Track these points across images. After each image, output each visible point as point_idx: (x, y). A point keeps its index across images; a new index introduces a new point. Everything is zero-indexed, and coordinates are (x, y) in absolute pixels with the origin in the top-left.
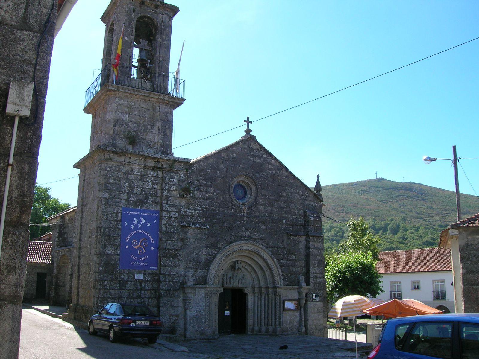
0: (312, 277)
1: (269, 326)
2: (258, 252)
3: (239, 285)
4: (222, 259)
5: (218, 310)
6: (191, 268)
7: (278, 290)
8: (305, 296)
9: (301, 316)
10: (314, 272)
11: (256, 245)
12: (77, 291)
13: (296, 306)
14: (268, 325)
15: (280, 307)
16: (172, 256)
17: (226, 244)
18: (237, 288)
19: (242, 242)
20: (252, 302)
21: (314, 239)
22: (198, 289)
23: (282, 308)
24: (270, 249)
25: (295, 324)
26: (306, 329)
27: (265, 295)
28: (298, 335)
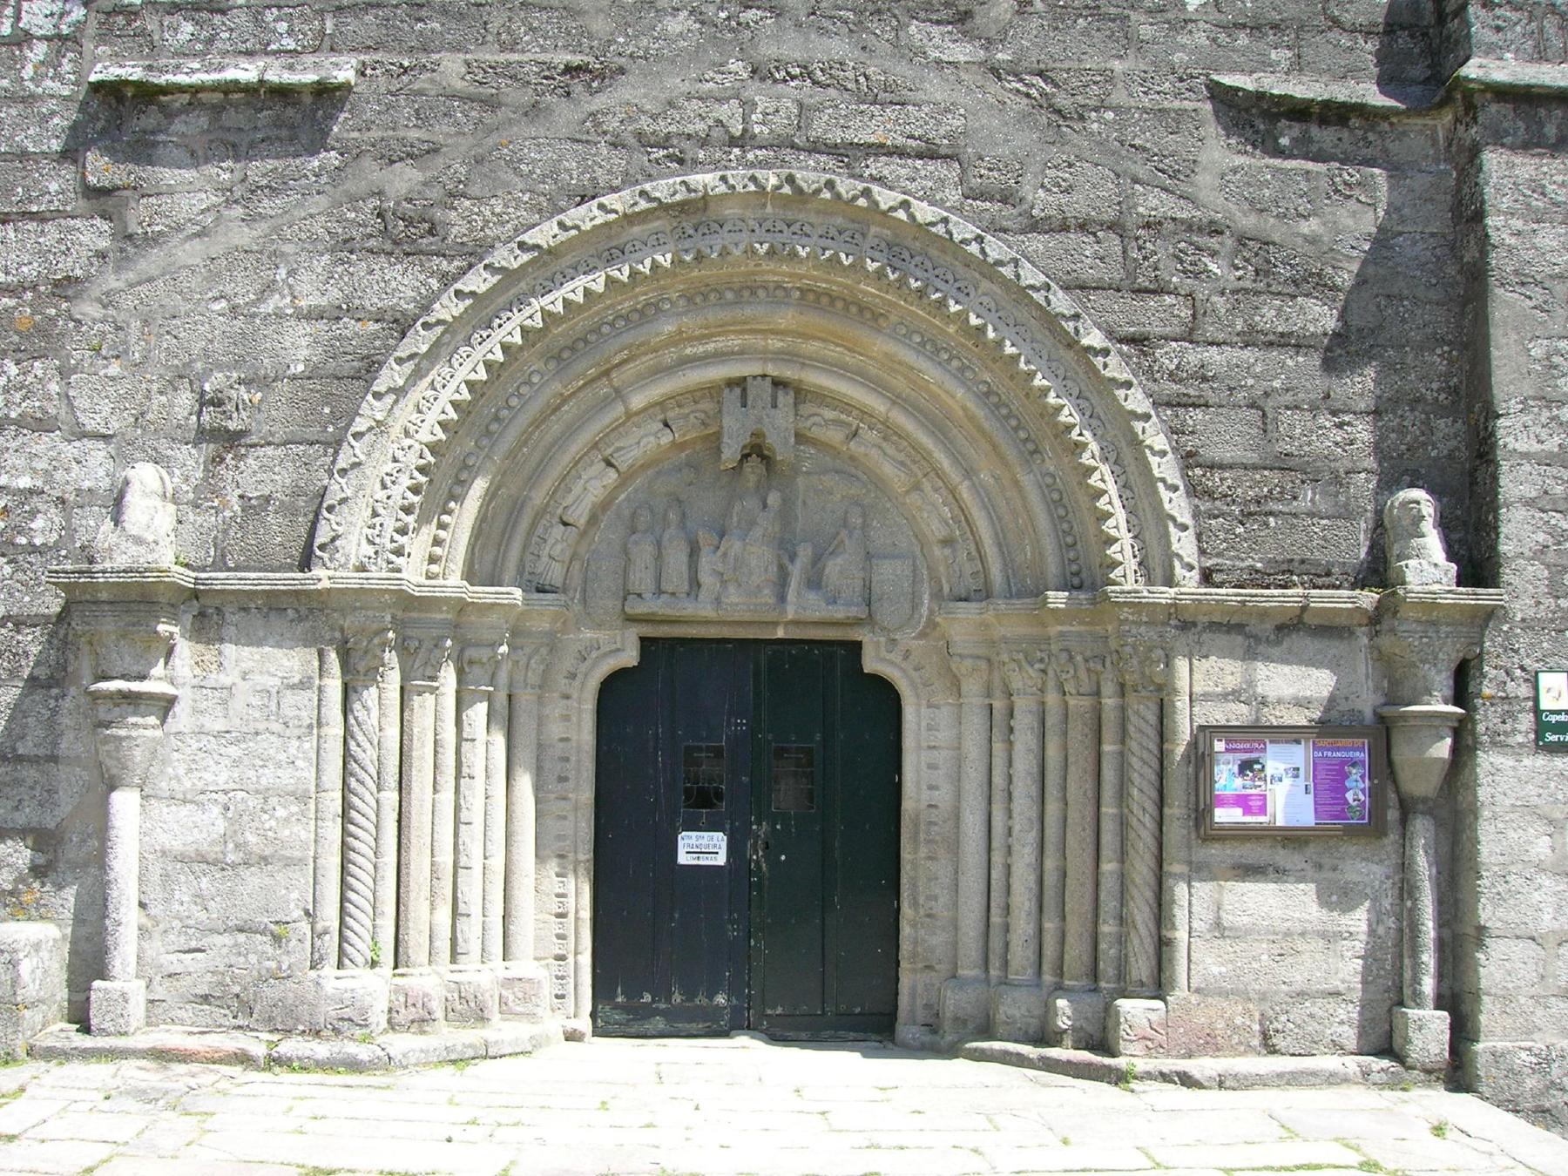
0: (1529, 503)
9: (1411, 896)
12: (991, 944)
16: (16, 338)
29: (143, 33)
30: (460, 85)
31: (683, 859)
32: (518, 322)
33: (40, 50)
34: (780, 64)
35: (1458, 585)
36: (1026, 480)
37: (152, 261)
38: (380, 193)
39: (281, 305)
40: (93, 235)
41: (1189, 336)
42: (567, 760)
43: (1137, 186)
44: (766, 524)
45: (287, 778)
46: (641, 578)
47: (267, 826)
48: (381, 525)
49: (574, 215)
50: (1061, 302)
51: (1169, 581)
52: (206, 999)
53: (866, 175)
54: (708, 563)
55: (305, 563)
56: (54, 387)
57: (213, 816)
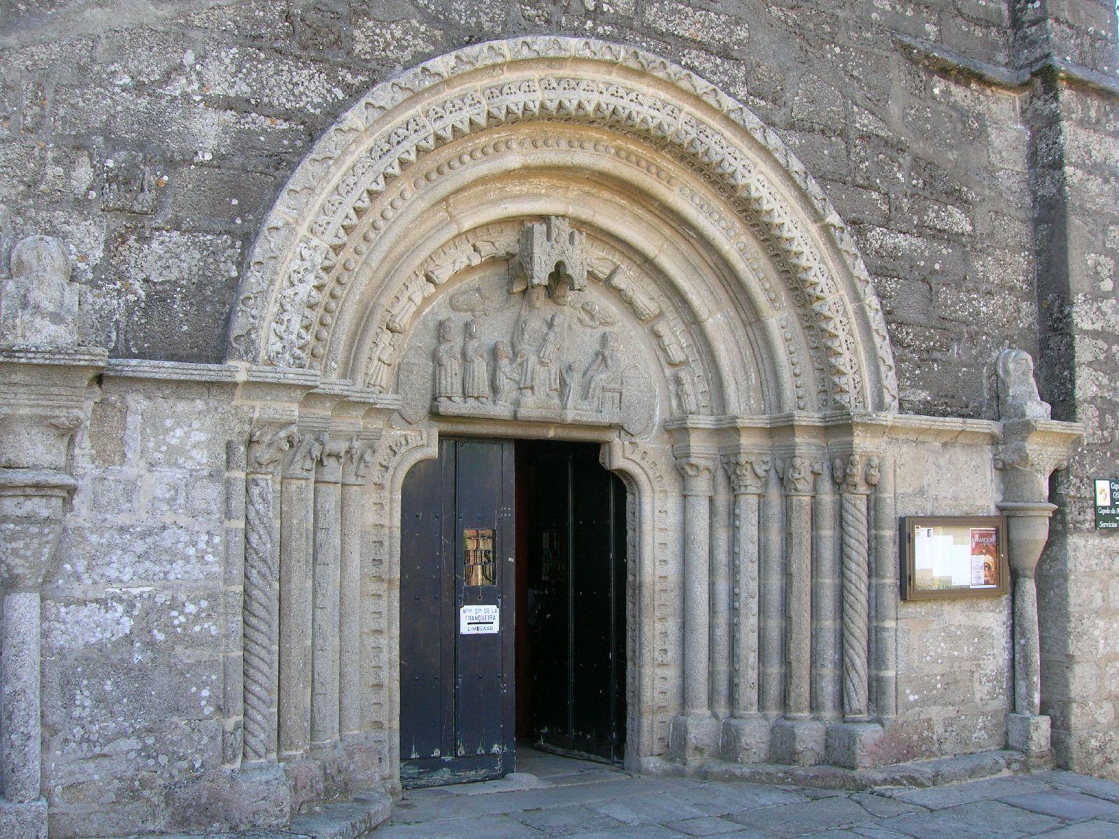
0: (1090, 364)
1: (795, 714)
2: (701, 150)
3: (565, 407)
4: (393, 158)
5: (396, 593)
6: (80, 204)
7: (863, 443)
8: (1046, 492)
9: (1023, 635)
10: (1098, 326)
11: (684, 84)
13: (987, 566)
14: (784, 702)
15: (874, 570)
17: (430, 40)
18: (551, 434)
19: (574, 45)
20: (672, 538)
21: (1086, 109)
22: (144, 404)
23: (890, 579)
24: (795, 139)
25: (981, 691)
26: (1060, 726)
27: (766, 485)
28: (1005, 773)
31: (465, 629)
32: (415, 142)
35: (1052, 418)
39: (189, 90)
42: (381, 543)
43: (855, 107)
47: (176, 622)
48: (289, 321)
53: (683, 63)
57: (118, 615)
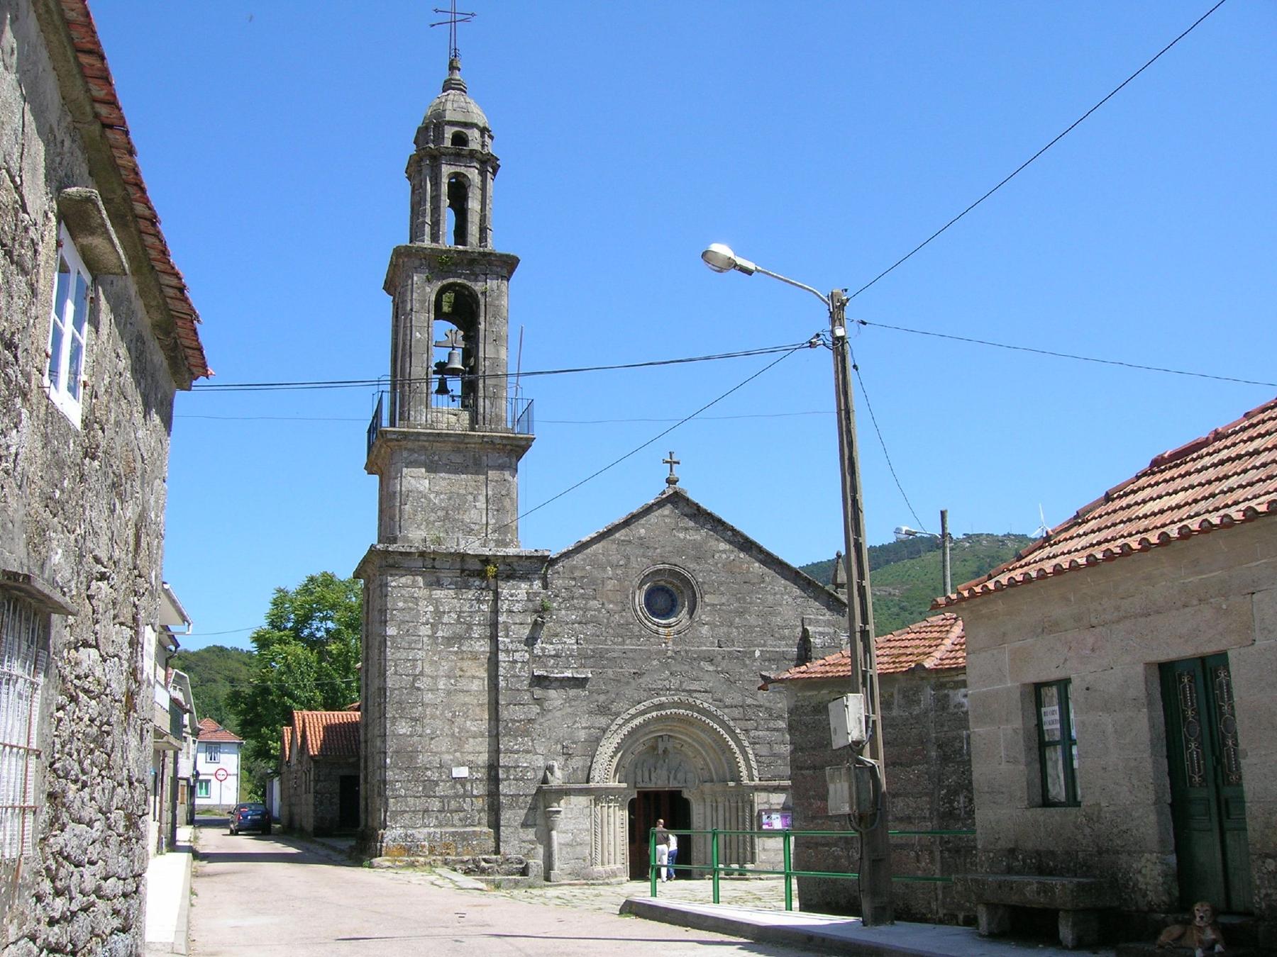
29: (543, 662)
30: (612, 677)
33: (519, 665)
34: (676, 672)
36: (723, 759)
37: (549, 716)
38: (597, 701)
40: (536, 709)
41: (756, 729)
44: (665, 767)
45: (585, 827)
46: (639, 779)
49: (638, 707)
50: (732, 724)
51: (753, 780)
52: (570, 874)
54: (653, 775)
55: (588, 781)
56: (530, 744)
